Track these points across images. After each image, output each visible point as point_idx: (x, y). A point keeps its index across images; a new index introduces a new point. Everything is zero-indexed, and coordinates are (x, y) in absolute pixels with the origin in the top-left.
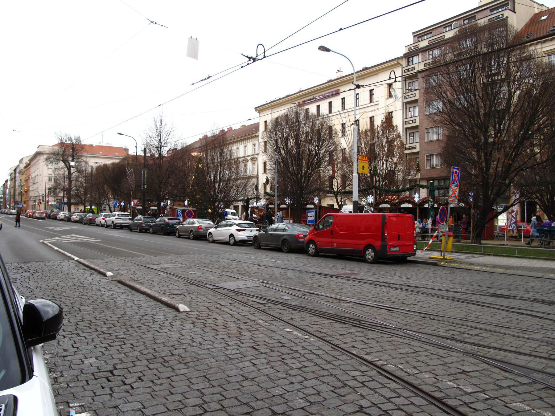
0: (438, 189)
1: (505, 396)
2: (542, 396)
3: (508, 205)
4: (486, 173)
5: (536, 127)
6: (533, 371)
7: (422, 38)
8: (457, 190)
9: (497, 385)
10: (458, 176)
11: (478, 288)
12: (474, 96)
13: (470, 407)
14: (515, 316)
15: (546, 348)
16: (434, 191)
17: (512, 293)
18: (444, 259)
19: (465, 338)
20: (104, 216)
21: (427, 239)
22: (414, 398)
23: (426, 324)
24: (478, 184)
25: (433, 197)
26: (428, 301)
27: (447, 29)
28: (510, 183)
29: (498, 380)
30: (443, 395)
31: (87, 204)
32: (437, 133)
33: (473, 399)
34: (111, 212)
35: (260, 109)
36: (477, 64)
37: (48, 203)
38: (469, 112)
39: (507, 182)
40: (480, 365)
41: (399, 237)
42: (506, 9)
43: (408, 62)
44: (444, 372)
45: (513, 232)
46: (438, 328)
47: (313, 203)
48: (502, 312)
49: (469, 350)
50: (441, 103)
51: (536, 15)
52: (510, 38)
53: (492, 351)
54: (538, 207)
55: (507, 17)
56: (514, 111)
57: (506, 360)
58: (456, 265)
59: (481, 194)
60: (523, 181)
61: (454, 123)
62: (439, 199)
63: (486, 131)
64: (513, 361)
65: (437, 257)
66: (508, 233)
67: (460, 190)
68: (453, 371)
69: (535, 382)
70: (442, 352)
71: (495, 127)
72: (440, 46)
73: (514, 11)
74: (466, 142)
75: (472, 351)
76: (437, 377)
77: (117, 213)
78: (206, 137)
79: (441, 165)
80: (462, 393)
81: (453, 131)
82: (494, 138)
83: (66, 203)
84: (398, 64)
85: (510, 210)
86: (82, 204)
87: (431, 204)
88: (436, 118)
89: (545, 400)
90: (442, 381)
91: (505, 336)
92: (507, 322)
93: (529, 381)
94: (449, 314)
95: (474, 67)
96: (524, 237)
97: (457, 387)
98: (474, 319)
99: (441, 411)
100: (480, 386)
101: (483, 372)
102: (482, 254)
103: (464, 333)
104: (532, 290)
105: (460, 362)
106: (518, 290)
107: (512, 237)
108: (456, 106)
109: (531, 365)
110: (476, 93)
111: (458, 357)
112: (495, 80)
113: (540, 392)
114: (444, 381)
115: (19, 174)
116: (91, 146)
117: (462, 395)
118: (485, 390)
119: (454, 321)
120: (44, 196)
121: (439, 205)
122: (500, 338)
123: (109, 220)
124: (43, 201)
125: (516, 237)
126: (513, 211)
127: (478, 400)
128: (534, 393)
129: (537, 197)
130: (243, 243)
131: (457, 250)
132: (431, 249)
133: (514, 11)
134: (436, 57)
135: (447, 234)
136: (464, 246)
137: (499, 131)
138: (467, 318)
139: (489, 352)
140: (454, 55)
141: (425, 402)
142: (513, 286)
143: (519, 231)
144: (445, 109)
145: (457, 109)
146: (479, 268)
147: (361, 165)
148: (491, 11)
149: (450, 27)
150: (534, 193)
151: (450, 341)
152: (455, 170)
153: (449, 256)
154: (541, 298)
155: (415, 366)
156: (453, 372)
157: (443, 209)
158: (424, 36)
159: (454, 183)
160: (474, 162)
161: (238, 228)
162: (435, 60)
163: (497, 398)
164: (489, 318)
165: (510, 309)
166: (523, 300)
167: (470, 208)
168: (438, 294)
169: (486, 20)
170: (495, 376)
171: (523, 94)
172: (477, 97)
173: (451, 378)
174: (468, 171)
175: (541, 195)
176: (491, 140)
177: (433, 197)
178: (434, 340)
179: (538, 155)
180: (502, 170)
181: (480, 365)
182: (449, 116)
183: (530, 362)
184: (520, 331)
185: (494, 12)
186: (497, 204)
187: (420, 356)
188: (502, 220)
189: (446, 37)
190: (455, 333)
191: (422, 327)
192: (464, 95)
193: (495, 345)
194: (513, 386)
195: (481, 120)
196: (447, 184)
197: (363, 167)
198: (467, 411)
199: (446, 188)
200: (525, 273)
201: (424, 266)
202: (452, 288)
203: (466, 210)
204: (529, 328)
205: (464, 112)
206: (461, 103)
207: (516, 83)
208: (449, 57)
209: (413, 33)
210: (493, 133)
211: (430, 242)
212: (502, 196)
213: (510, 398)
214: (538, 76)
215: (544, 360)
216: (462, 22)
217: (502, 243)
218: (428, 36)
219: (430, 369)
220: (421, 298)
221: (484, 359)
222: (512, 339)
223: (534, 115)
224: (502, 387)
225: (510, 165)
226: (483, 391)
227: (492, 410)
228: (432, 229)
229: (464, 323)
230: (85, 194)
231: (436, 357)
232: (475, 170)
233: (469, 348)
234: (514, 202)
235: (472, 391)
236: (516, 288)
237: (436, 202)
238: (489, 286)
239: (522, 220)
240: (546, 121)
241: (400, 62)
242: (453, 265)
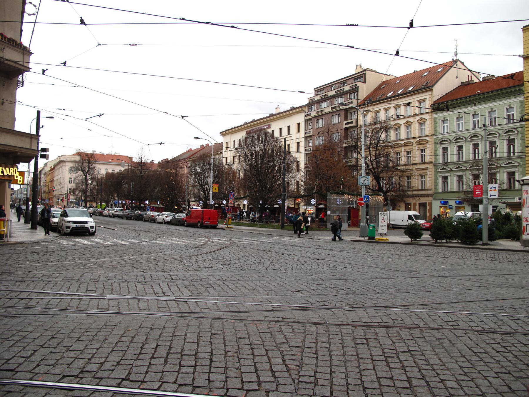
20: (109, 210)
31: (99, 201)
34: (112, 208)
35: (224, 134)
37: (69, 200)
41: (209, 218)
43: (309, 109)
47: (278, 204)
55: (359, 87)
77: (116, 208)
78: (190, 150)
83: (83, 201)
84: (302, 111)
86: (95, 201)
115: (44, 175)
116: (102, 155)
120: (67, 195)
123: (111, 213)
124: (66, 199)
130: (168, 223)
147: (214, 188)
148: (355, 80)
158: (320, 91)
161: (166, 216)
197: (215, 189)
209: (315, 89)
230: (98, 194)
241: (304, 109)
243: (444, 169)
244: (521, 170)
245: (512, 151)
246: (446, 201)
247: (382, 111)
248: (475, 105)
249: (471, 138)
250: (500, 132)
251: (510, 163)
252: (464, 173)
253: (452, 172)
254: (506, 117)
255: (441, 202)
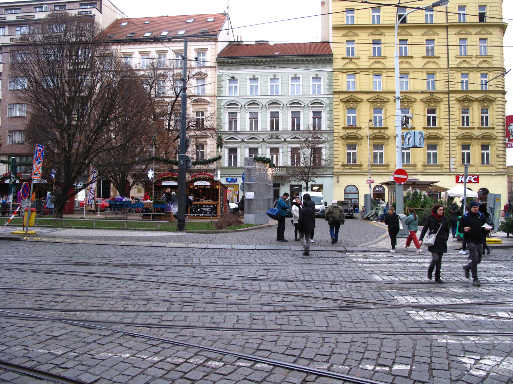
0: (20, 165)
1: (91, 350)
2: (121, 343)
3: (87, 183)
4: (68, 153)
5: (113, 116)
6: (113, 324)
7: (10, 12)
8: (41, 167)
9: (85, 342)
10: (42, 153)
11: (61, 259)
12: (61, 80)
13: (62, 368)
14: (96, 280)
15: (122, 302)
16: (16, 167)
17: (92, 260)
18: (26, 234)
19: (53, 306)
21: (7, 215)
22: (4, 374)
23: (12, 299)
24: (61, 162)
25: (15, 173)
26: (12, 276)
27: (38, 10)
28: (89, 163)
29: (85, 337)
30: (34, 363)
32: (21, 110)
33: (63, 360)
36: (65, 51)
38: (55, 94)
39: (87, 162)
40: (68, 328)
42: (94, 8)
44: (34, 342)
45: (91, 207)
46: (25, 301)
48: (84, 278)
49: (57, 316)
50: (26, 81)
51: (118, 20)
52: (96, 34)
53: (78, 313)
54: (112, 184)
55: (94, 15)
56: (96, 100)
57: (90, 319)
58: (39, 239)
59: (63, 171)
60: (100, 162)
61: (39, 102)
62: (21, 175)
63: (70, 113)
64: (96, 319)
65: (19, 232)
66: (87, 208)
67: (43, 167)
68: (43, 338)
69: (115, 332)
70: (30, 323)
71: (78, 112)
72: (29, 24)
73: (100, 11)
74: (51, 123)
75: (60, 317)
76: (27, 348)
79: (23, 142)
80: (53, 357)
81: (39, 110)
82: (77, 121)
85: (89, 187)
87: (13, 180)
88: (21, 95)
89: (124, 345)
90: (33, 350)
91: (88, 298)
92: (89, 286)
93: (111, 332)
94: (34, 286)
95: (63, 53)
96: (100, 211)
97: (48, 353)
98: (60, 287)
99: (34, 379)
100: (70, 346)
101: (71, 334)
102: (64, 227)
103: (51, 301)
104: (108, 256)
105: (49, 329)
106: (97, 257)
107: (90, 211)
108: (42, 86)
109: (111, 319)
110: (63, 78)
111: (46, 325)
112: (80, 69)
113: (119, 339)
114: (35, 350)
117: (53, 359)
118: (74, 349)
119: (40, 292)
121: (22, 181)
122: (84, 301)
125: (93, 211)
126: (91, 188)
127: (68, 360)
128: (115, 341)
129: (112, 177)
131: (39, 224)
132: (13, 224)
133: (100, 11)
134: (25, 35)
135: (30, 210)
136: (46, 221)
137: (81, 116)
138: (53, 287)
139: (75, 315)
140: (44, 37)
141: (17, 375)
142: (92, 254)
143: (96, 206)
144: (31, 88)
145: (43, 89)
146: (61, 240)
149: (40, 9)
150: (109, 172)
151: (37, 312)
152: (39, 148)
153: (31, 231)
154: (116, 262)
155: (3, 342)
156: (42, 340)
157: (26, 185)
158: (12, 9)
159: (37, 160)
160: (58, 142)
162: (23, 38)
163: (85, 353)
164: (74, 285)
165: (91, 275)
166: (101, 265)
167: (52, 185)
168: (21, 268)
169: (76, 11)
170: (82, 335)
171: (105, 85)
172: (64, 81)
173: (42, 345)
174: (51, 150)
175: (115, 175)
176: (74, 123)
177: (15, 173)
178: (22, 313)
179: (114, 140)
180: (83, 150)
181: (68, 328)
182: (35, 95)
183: (110, 317)
184: (100, 292)
185: (83, 7)
186: (78, 182)
187: (7, 331)
188: (81, 196)
189: (36, 18)
190: (42, 303)
191: (7, 303)
192: (51, 77)
193: (80, 308)
194: (98, 340)
195: (65, 103)
196: (29, 161)
198: (59, 372)
199: (29, 165)
200: (102, 242)
201: (5, 241)
202: (36, 261)
203: (49, 187)
204: (109, 288)
205: (51, 94)
206: (47, 84)
207: (99, 75)
208: (39, 38)
210: (76, 116)
211: (11, 218)
212: (82, 174)
213: (96, 350)
214: (117, 72)
215: (121, 313)
216: (53, 7)
217: (81, 216)
218: (17, 11)
219: (19, 342)
220: (4, 273)
221: (71, 322)
222: (94, 300)
223: (112, 105)
224: (88, 343)
225: (90, 147)
226: (73, 351)
227: (82, 364)
228: (13, 205)
229: (51, 292)
231: (26, 329)
232: (58, 148)
233: (56, 314)
234: (93, 180)
235: (63, 352)
236: (95, 256)
237: (18, 178)
238: (71, 256)
239: (99, 196)
240: (122, 111)
242: (35, 239)
243: (232, 138)
244: (328, 146)
245: (485, 122)
246: (234, 178)
247: (136, 55)
248: (275, 67)
249: (290, 105)
250: (285, 103)
251: (253, 138)
252: (260, 145)
253: (264, 144)
254: (479, 82)
255: (227, 179)
